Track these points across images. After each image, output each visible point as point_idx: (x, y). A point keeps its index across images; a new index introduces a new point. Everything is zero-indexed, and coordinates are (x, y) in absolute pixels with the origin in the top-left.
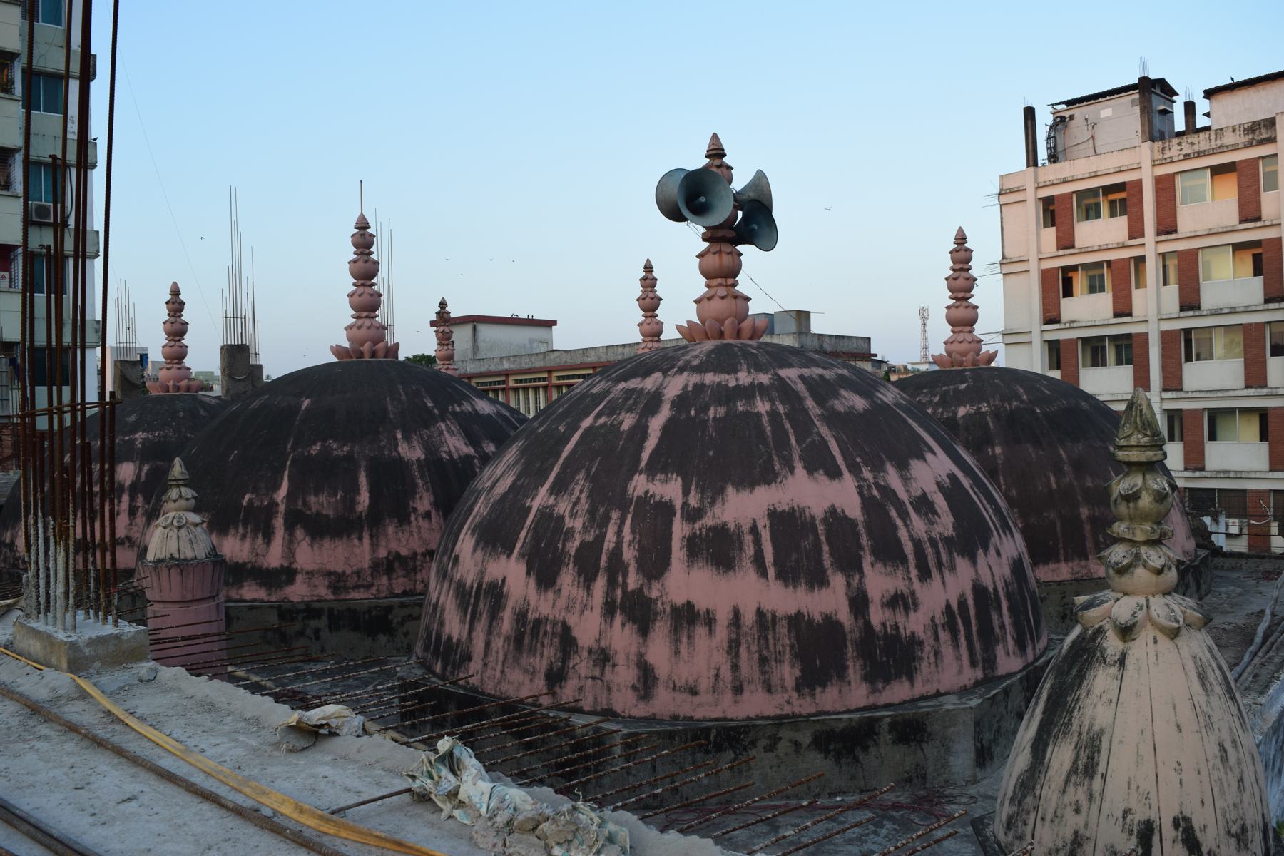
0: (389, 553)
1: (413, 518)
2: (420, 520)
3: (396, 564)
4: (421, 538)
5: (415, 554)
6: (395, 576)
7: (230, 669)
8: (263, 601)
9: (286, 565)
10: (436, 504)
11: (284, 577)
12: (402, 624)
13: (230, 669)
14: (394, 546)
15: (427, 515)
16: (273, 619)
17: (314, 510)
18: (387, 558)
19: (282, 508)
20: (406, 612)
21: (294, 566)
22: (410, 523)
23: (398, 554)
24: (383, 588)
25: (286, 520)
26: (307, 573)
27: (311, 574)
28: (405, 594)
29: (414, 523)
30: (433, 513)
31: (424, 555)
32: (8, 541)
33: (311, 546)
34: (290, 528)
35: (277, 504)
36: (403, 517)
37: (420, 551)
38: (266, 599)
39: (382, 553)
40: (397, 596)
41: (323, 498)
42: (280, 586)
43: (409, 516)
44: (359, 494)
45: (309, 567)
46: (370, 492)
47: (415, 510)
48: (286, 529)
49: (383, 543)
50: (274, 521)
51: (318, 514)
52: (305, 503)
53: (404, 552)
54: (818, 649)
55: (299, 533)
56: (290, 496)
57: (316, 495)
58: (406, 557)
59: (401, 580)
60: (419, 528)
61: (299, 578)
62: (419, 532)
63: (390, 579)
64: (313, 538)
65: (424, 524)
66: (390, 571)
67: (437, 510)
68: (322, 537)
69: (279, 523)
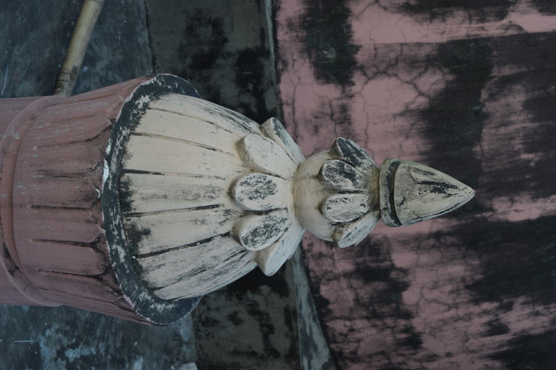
0: (405, 271)
1: (486, 306)
2: (486, 319)
3: (380, 286)
4: (445, 322)
5: (408, 316)
6: (355, 283)
7: (13, 364)
8: (275, 10)
9: (360, 57)
10: (525, 339)
11: (331, 55)
12: (254, 311)
13: (13, 364)
14: (421, 279)
15: (497, 328)
16: (239, 40)
17: (490, 107)
18: (392, 267)
19: (493, 29)
20: (278, 320)
21: (358, 78)
22: (476, 302)
23: (405, 286)
24: (326, 265)
25: (461, 44)
26: (344, 109)
27: (343, 117)
28: (321, 306)
29: (475, 309)
30: (499, 338)
31: (408, 330)
32: (136, 104)
33: (406, 112)
34: (446, 56)
35: (501, 15)
36: (489, 288)
37: (417, 323)
38: (281, 18)
39: (401, 259)
40: (314, 289)
41: (522, 122)
42: (310, 48)
43: (491, 298)
44: (535, 198)
45: (358, 111)
46: (542, 220)
47: (508, 307)
48: (442, 47)
49: (424, 258)
50: (460, 14)
51: (482, 117)
52: (506, 82)
53: (409, 297)
54: (510, 163)
55: (433, 81)
56: (527, 40)
57: (527, 105)
58: (399, 301)
59: (349, 295)
60: (468, 317)
61: (331, 92)
62: (457, 319)
63: (347, 275)
64: (425, 114)
65: (478, 324)
66: (365, 274)
67: (510, 342)
68: (429, 133)
69: (457, 27)
